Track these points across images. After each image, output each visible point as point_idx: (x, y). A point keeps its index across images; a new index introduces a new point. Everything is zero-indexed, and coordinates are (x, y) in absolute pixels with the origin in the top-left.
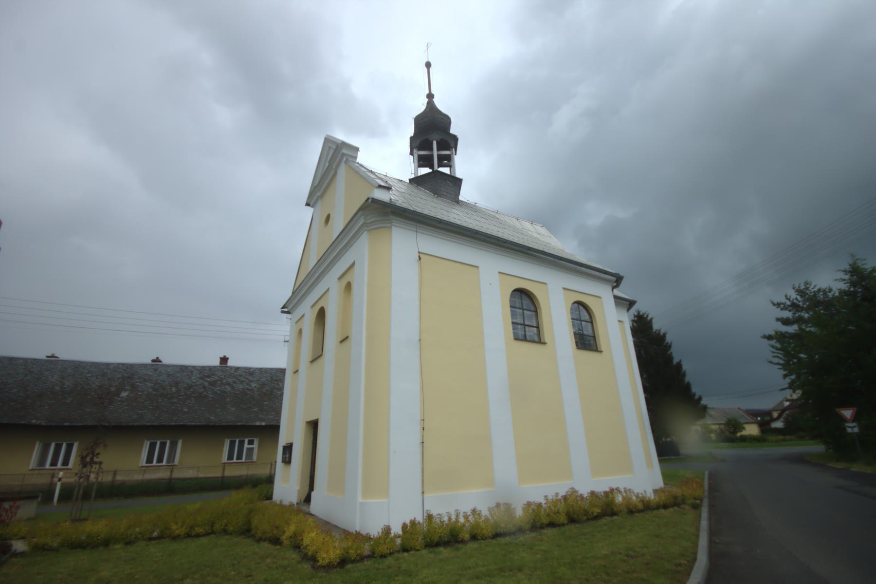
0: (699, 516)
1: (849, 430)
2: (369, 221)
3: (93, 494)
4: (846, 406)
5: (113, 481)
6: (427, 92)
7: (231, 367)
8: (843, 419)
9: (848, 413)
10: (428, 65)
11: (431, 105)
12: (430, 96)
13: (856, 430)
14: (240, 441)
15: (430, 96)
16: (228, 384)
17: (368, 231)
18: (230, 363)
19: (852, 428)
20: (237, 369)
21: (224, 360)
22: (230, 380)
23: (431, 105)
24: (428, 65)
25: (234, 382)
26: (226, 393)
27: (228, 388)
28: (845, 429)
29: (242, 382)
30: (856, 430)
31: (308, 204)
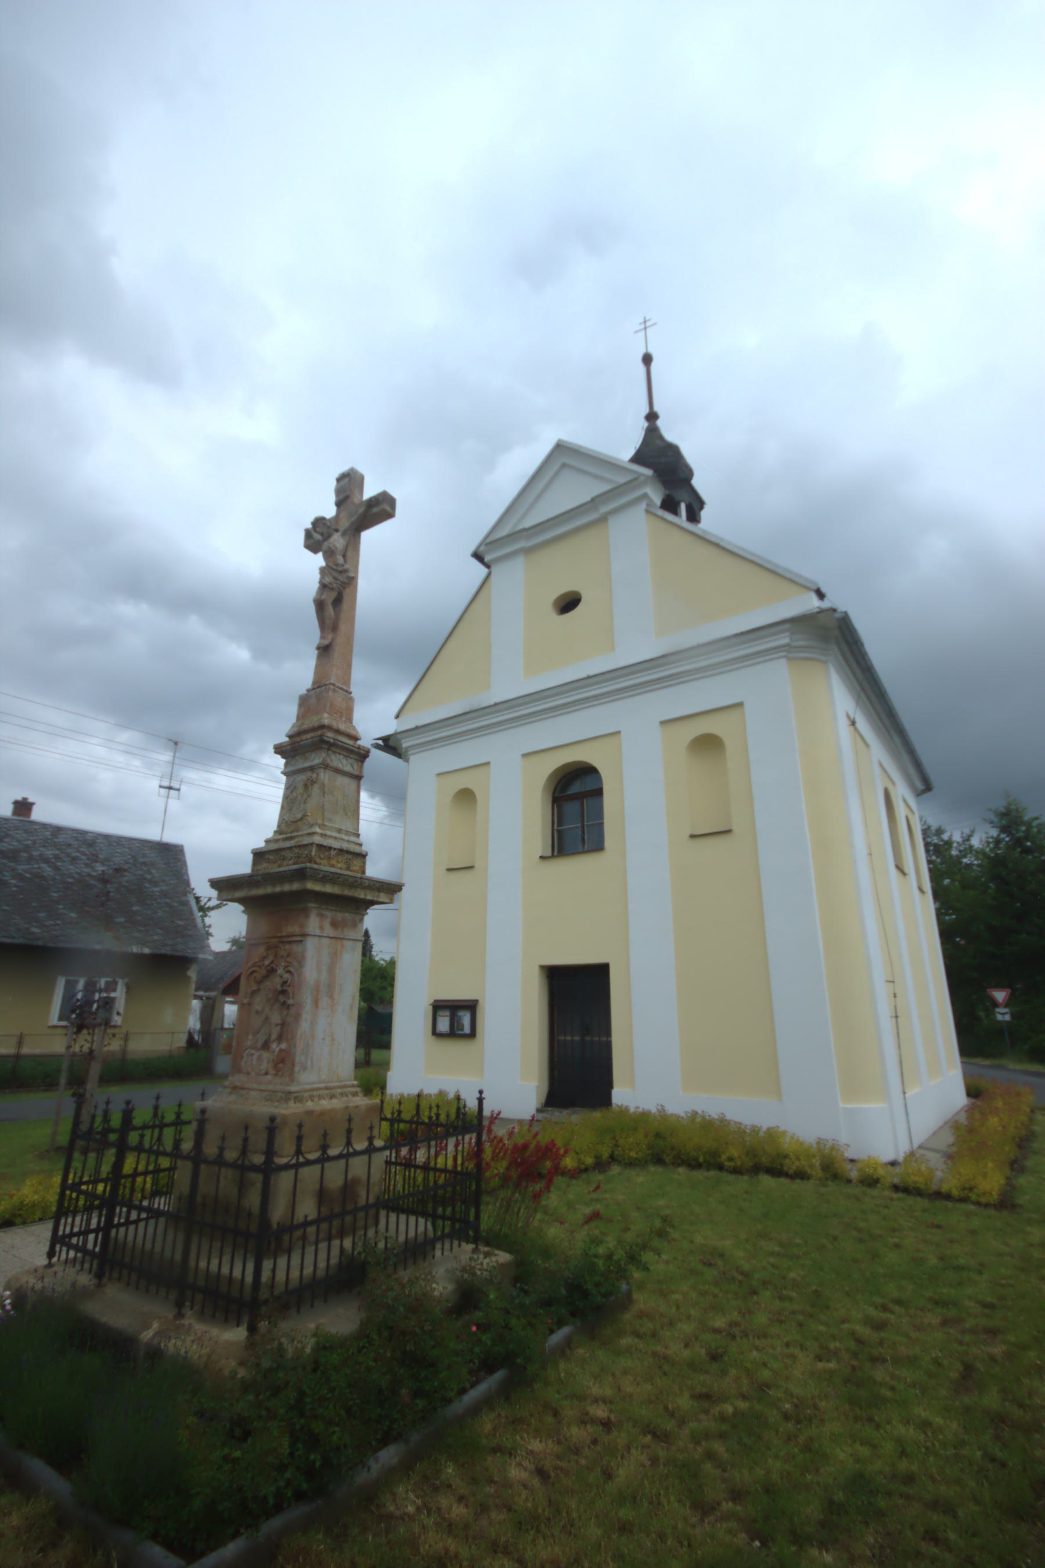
0: (462, 1164)
1: (999, 1017)
2: (795, 644)
3: (63, 1081)
4: (1000, 986)
5: (124, 1052)
6: (645, 410)
7: (34, 823)
8: (995, 1004)
9: (1000, 996)
10: (647, 359)
11: (652, 432)
12: (652, 417)
13: (1007, 1018)
14: (68, 982)
15: (652, 417)
16: (46, 861)
17: (789, 659)
18: (38, 815)
19: (1003, 1015)
20: (45, 826)
21: (23, 807)
22: (49, 853)
23: (652, 432)
24: (647, 359)
25: (57, 857)
26: (43, 878)
27: (48, 870)
28: (994, 1014)
29: (74, 859)
30: (1007, 1018)
31: (478, 556)
